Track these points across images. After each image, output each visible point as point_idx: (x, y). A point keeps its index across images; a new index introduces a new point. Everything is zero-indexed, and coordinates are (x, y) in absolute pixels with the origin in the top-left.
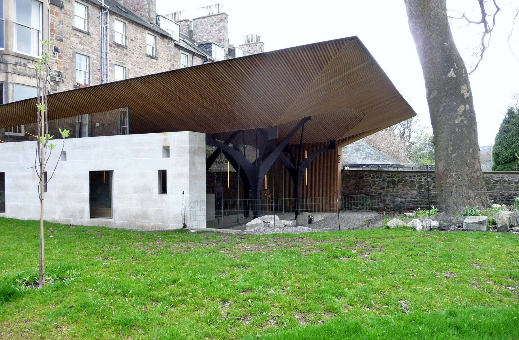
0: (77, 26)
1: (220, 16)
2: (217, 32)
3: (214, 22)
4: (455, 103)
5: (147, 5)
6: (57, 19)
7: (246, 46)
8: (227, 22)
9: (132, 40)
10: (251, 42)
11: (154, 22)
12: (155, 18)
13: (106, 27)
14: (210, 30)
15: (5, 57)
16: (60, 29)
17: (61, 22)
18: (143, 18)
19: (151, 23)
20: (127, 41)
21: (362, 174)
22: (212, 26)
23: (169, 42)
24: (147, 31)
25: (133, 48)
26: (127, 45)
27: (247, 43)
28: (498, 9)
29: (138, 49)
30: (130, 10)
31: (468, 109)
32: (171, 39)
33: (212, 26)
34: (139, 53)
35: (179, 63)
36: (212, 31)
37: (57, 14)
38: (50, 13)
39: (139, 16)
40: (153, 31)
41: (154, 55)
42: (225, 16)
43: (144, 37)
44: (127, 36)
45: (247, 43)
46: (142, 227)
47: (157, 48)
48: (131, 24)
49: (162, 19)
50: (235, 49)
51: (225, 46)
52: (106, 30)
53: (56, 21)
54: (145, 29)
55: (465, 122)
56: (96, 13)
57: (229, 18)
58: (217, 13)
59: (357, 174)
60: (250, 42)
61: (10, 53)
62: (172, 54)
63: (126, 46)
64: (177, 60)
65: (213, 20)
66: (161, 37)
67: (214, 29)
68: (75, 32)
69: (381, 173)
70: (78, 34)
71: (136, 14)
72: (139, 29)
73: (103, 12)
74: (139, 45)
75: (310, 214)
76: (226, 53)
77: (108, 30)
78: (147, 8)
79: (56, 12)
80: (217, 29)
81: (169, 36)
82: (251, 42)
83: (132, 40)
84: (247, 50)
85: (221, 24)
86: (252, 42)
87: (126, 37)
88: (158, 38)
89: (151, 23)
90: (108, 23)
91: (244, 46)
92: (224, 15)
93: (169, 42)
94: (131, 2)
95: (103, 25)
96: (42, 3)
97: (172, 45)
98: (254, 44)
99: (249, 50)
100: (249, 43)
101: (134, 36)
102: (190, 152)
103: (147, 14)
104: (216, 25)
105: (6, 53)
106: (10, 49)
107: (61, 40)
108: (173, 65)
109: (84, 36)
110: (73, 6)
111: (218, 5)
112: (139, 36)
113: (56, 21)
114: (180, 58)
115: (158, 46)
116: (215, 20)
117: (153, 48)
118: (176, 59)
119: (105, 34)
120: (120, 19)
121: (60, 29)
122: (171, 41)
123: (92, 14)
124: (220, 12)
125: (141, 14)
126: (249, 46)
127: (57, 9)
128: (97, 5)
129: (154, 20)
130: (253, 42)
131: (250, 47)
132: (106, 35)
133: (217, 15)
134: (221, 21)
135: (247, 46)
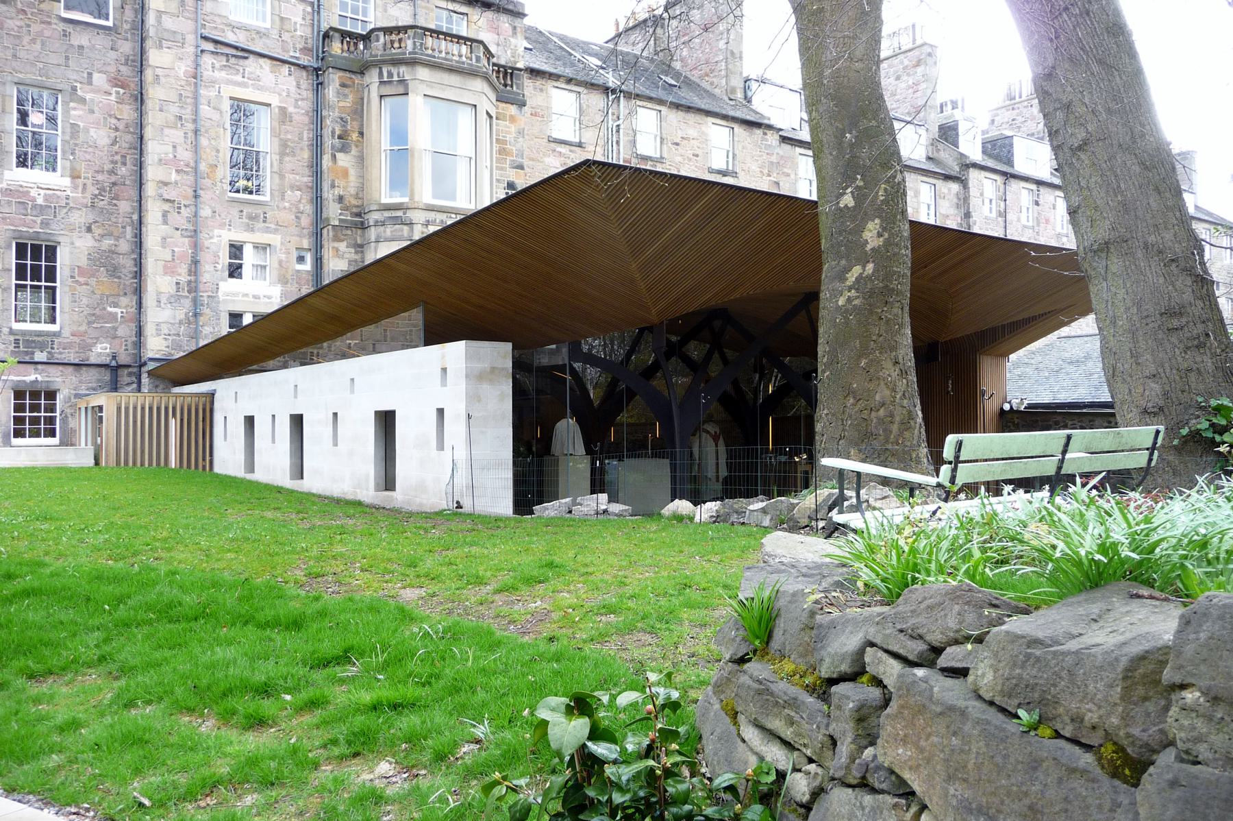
0: (556, 135)
1: (916, 53)
2: (911, 91)
3: (904, 69)
4: (843, 262)
5: (723, 64)
6: (513, 129)
7: (1004, 110)
8: (935, 63)
9: (677, 144)
10: (1018, 100)
11: (739, 95)
12: (742, 86)
13: (618, 126)
14: (894, 89)
15: (410, 214)
16: (518, 146)
17: (521, 133)
18: (717, 91)
19: (731, 100)
20: (665, 147)
21: (1048, 421)
22: (898, 78)
23: (765, 134)
24: (711, 120)
25: (679, 159)
26: (665, 155)
27: (1008, 102)
28: (475, 106)
29: (690, 160)
30: (692, 78)
31: (870, 272)
32: (770, 127)
33: (898, 78)
34: (693, 167)
35: (793, 176)
36: (898, 91)
37: (513, 119)
38: (45, 194)
39: (708, 88)
40: (725, 117)
41: (730, 168)
42: (929, 50)
43: (703, 133)
44: (664, 136)
45: (1008, 102)
46: (421, 505)
47: (737, 152)
48: (675, 111)
49: (754, 85)
50: (957, 125)
51: (929, 122)
52: (618, 131)
53: (509, 133)
54: (707, 116)
55: (856, 302)
56: (596, 101)
57: (939, 53)
58: (910, 46)
59: (1037, 421)
60: (1014, 99)
61: (416, 205)
62: (774, 159)
63: (662, 158)
64: (789, 171)
65: (902, 63)
66: (744, 127)
67: (903, 85)
68: (553, 145)
69: (1091, 418)
70: (559, 149)
71: (704, 84)
72: (692, 118)
73: (610, 98)
74: (692, 152)
75: (249, 476)
76: (931, 137)
77: (621, 131)
78: (723, 67)
79: (511, 116)
80: (910, 83)
81: (766, 121)
82: (1018, 100)
83: (677, 144)
84: (1006, 120)
85: (920, 70)
86: (1020, 97)
87: (662, 139)
88: (738, 129)
89: (731, 100)
90: (621, 117)
91: (999, 112)
92: (925, 47)
93: (765, 134)
94: (694, 62)
95: (611, 122)
96: (475, 106)
97: (772, 138)
98: (1026, 103)
99: (1013, 120)
100: (1013, 102)
101: (680, 134)
102: (467, 376)
103: (724, 81)
104: (908, 75)
105: (410, 206)
106: (417, 198)
107: (521, 167)
108: (777, 184)
109: (571, 151)
110: (549, 97)
111: (914, 26)
112: (692, 133)
113: (509, 133)
114: (795, 167)
115: (738, 147)
116: (906, 62)
117: (728, 152)
118: (785, 170)
119: (615, 139)
120: (649, 105)
121: (518, 146)
122: (769, 133)
123: (588, 106)
124: (918, 42)
125: (712, 84)
126: (1013, 109)
127: (513, 109)
128: (598, 86)
129: (738, 91)
130: (1024, 98)
131: (1016, 111)
132: (618, 142)
133: (910, 50)
134: (918, 64)
135: (1008, 110)
